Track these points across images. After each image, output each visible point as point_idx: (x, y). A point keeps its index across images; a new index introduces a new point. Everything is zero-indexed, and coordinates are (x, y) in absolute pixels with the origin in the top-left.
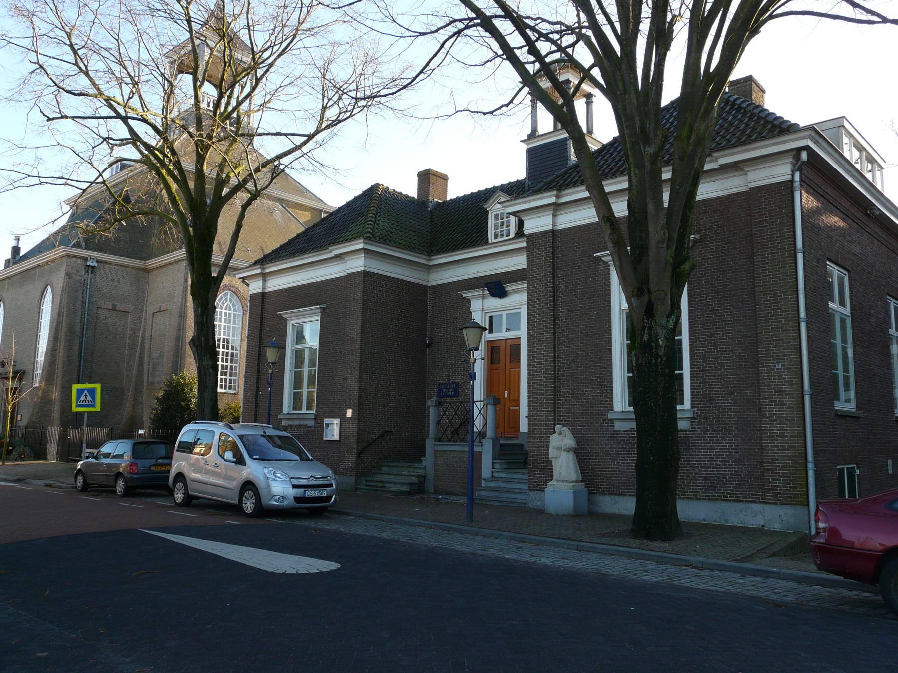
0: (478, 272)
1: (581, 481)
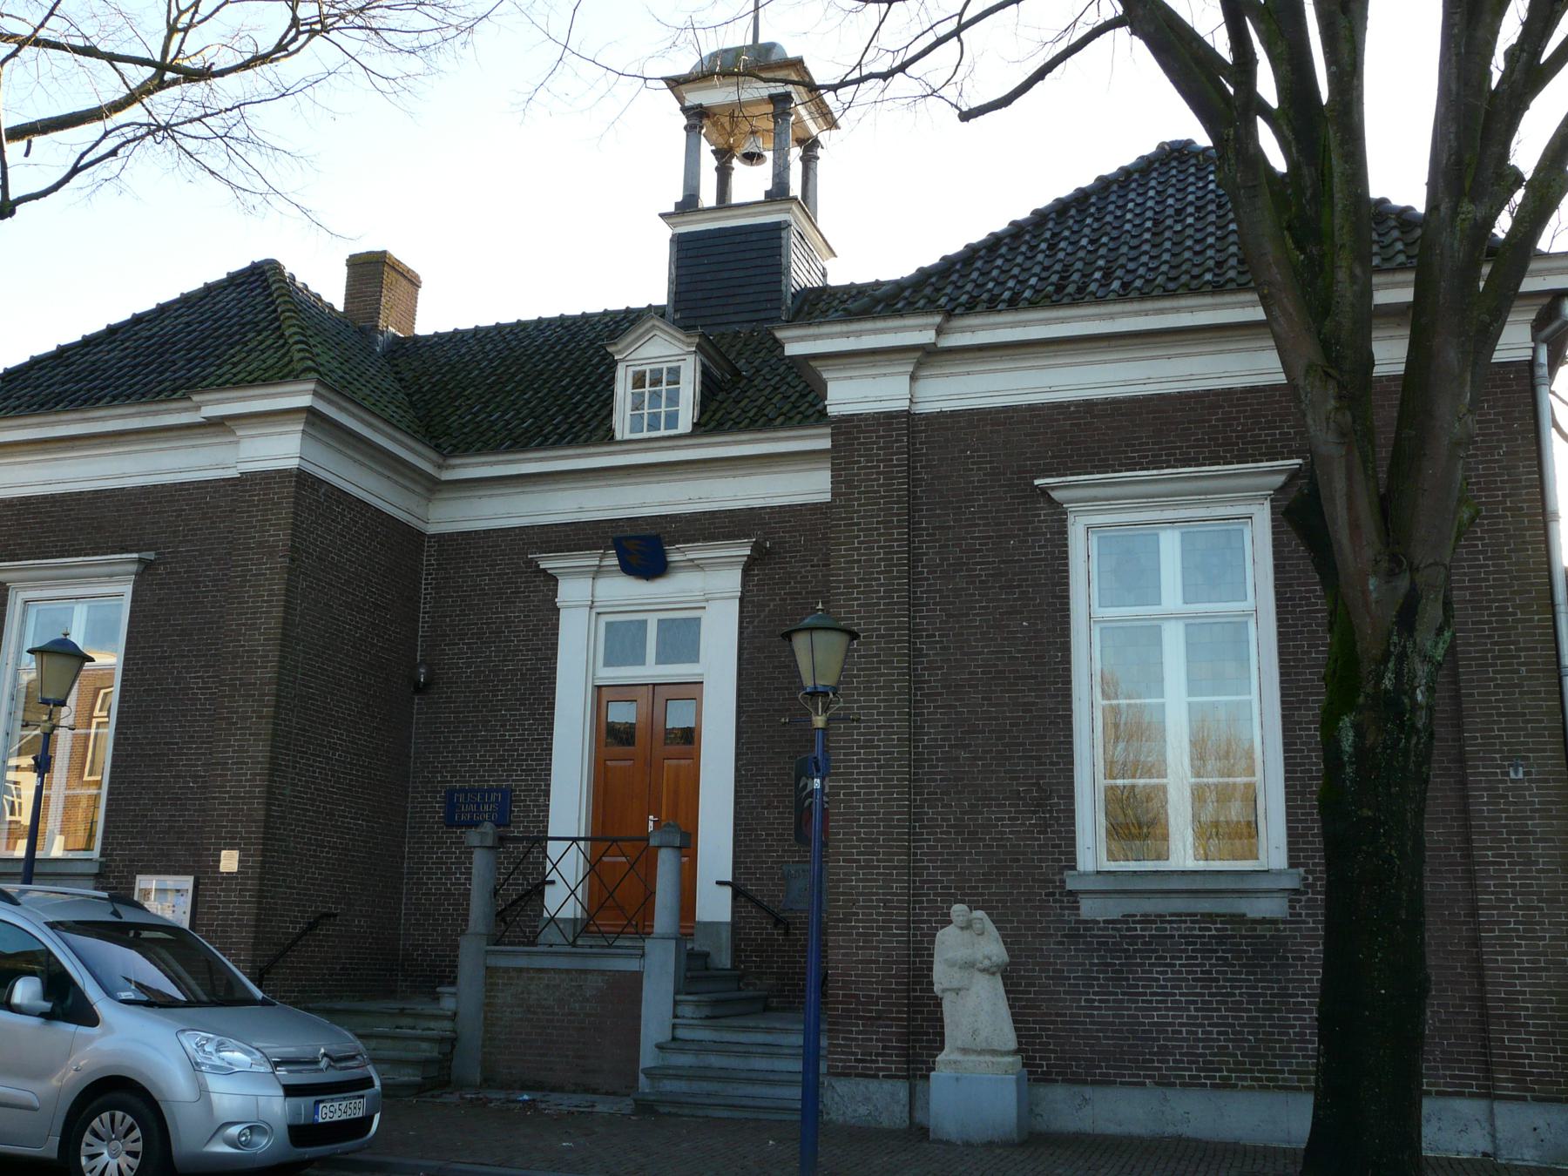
0: (581, 510)
1: (1017, 1052)
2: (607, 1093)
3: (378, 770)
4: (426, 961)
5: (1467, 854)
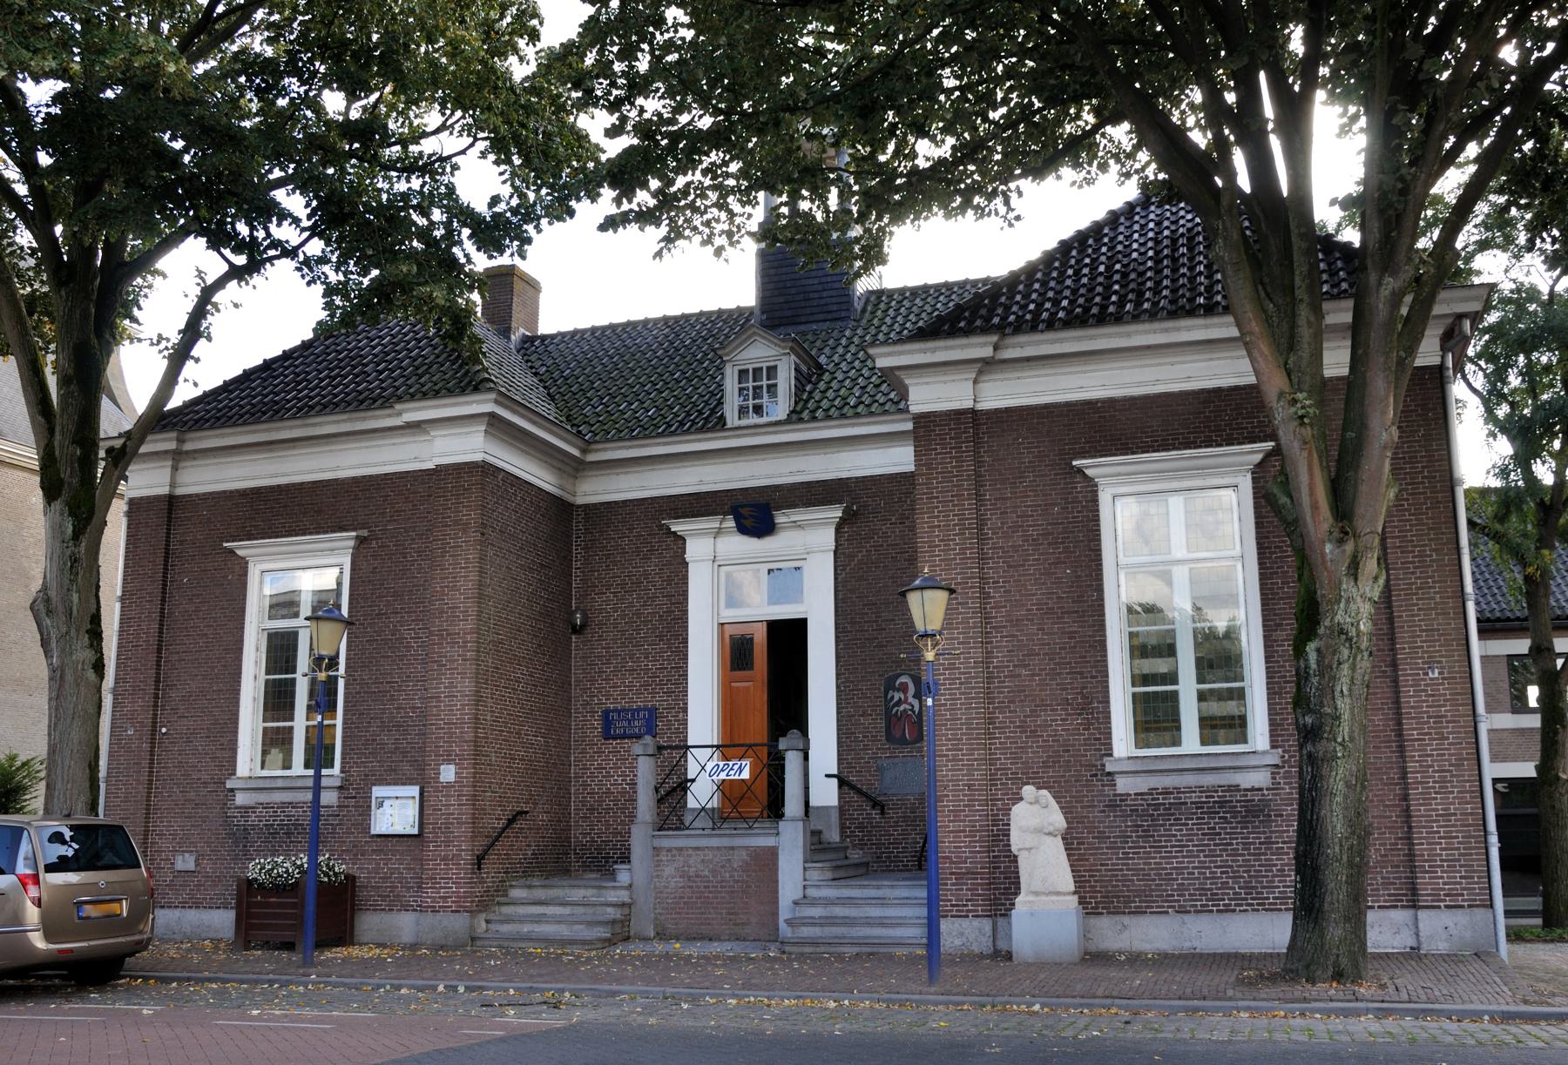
1: (1075, 893)
5: (1400, 734)
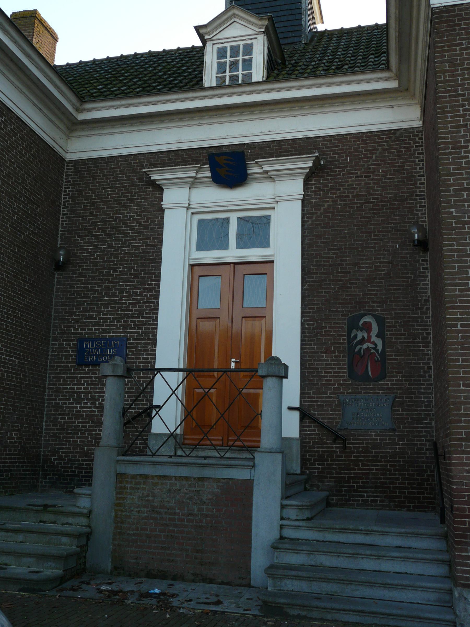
2: (222, 583)
3: (28, 322)
4: (61, 464)
